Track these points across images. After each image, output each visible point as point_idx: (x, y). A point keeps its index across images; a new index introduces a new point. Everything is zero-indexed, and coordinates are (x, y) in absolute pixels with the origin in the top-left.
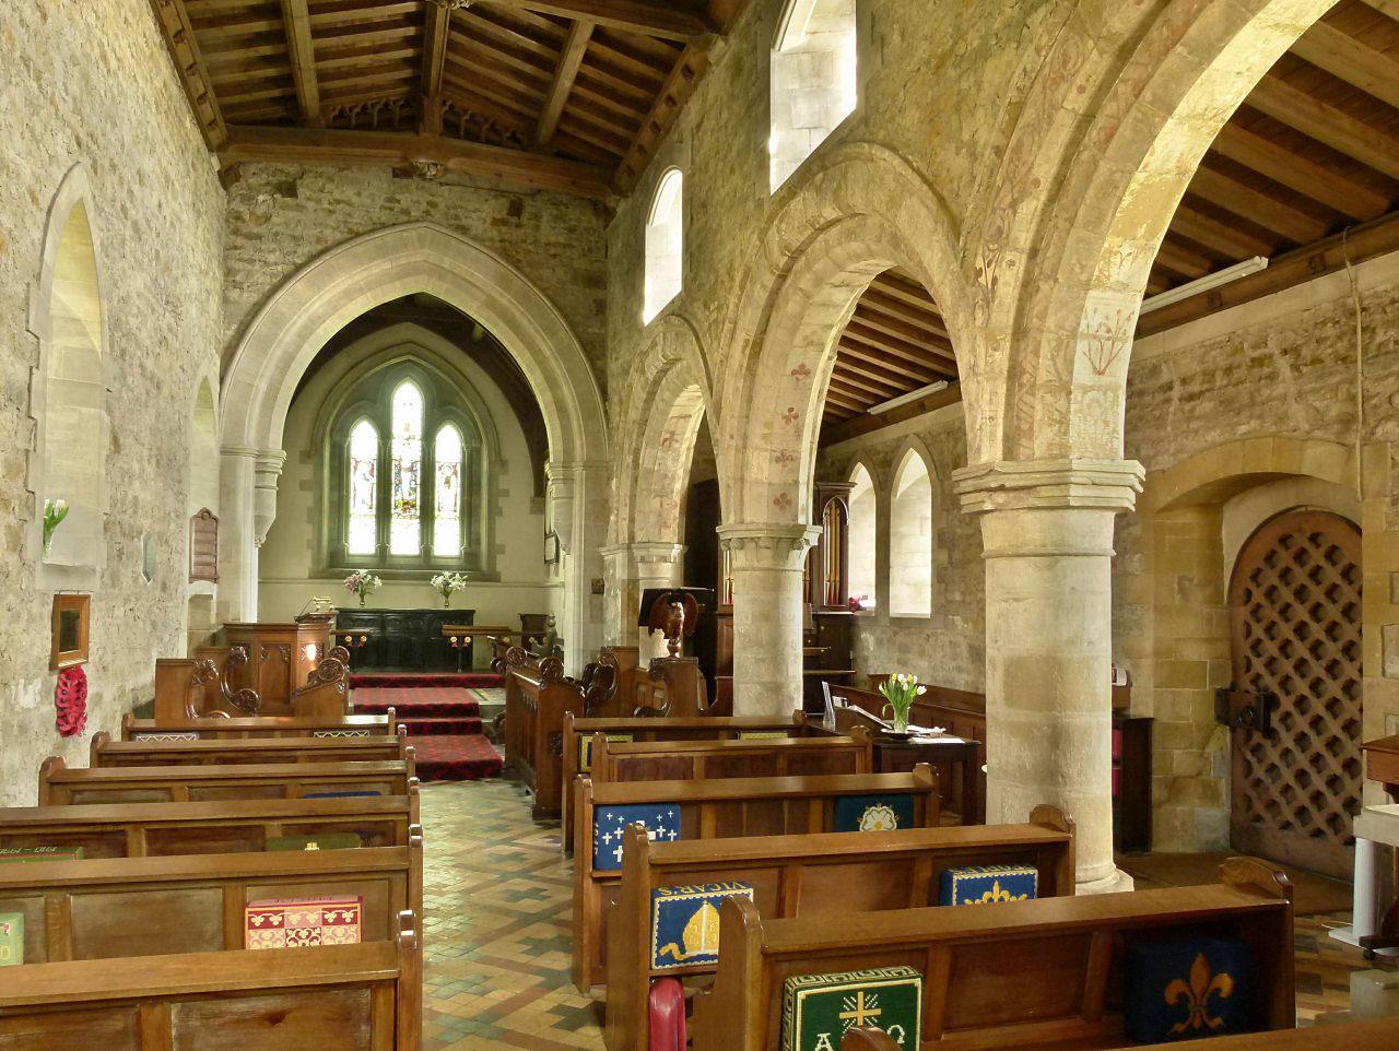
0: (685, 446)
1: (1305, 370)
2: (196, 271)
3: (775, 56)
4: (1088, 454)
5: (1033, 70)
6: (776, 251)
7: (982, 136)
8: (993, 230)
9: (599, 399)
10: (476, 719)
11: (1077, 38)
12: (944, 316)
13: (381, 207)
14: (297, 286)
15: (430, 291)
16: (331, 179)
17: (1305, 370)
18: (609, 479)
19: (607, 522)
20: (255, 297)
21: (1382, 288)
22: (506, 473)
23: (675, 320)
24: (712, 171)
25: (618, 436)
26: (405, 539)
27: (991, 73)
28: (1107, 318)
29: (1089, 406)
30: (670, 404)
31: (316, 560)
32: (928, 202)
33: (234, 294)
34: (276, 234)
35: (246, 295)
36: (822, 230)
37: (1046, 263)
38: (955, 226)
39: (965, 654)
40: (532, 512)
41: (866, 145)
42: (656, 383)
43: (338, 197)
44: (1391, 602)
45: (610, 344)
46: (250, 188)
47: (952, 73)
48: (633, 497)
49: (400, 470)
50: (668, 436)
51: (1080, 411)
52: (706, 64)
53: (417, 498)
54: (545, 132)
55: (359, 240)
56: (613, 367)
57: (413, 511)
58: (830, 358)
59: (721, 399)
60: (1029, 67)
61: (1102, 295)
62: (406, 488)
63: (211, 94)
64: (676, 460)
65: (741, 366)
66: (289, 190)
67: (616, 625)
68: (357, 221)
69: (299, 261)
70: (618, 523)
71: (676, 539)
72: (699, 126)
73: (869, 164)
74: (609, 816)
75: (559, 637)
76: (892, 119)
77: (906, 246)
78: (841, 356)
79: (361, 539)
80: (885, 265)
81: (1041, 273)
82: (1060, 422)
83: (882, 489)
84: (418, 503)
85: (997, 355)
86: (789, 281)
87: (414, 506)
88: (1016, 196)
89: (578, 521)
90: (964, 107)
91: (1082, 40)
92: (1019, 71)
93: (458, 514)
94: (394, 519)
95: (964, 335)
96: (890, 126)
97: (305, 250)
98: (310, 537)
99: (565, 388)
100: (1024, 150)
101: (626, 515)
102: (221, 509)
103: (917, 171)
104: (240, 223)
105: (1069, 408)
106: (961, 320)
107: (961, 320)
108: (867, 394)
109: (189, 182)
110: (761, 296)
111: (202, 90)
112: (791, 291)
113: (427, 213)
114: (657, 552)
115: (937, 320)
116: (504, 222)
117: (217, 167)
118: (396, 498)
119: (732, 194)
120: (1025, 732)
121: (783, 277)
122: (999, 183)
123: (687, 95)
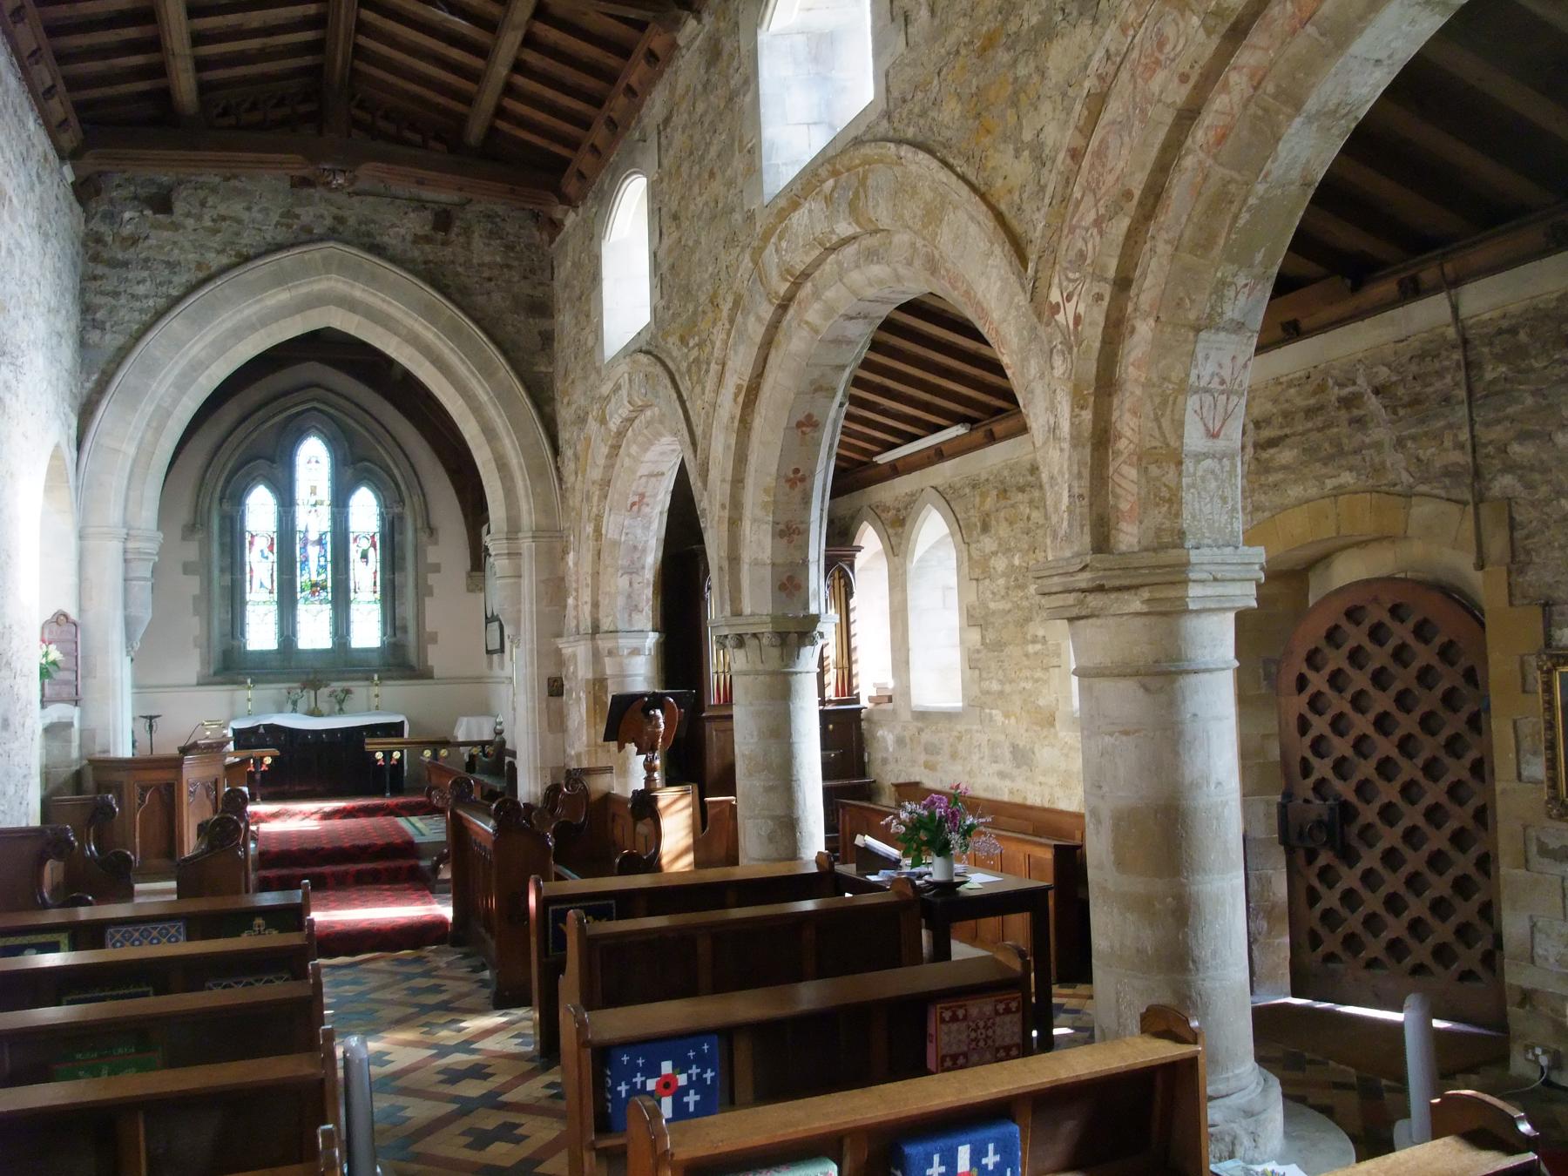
0: (658, 509)
1: (1401, 412)
2: (43, 309)
3: (763, 37)
4: (1206, 541)
5: (1117, 54)
6: (774, 274)
7: (1051, 135)
8: (1072, 254)
9: (548, 453)
10: (412, 862)
11: (1175, 13)
12: (1005, 360)
13: (278, 224)
14: (173, 324)
15: (337, 324)
16: (214, 190)
17: (1401, 412)
18: (565, 552)
19: (565, 607)
20: (120, 340)
21: (1486, 316)
22: (436, 543)
23: (644, 359)
24: (685, 176)
25: (575, 500)
26: (314, 632)
27: (1059, 57)
28: (1220, 366)
29: (1203, 479)
30: (637, 460)
31: (205, 662)
32: (981, 218)
33: (94, 336)
34: (146, 260)
35: (108, 337)
36: (833, 249)
37: (1143, 298)
38: (1018, 247)
39: (1008, 756)
40: (469, 590)
41: (892, 145)
42: (621, 434)
43: (223, 212)
44: (1524, 691)
45: (559, 385)
46: (111, 201)
47: (1004, 57)
48: (596, 574)
49: (305, 546)
50: (636, 499)
51: (1193, 485)
52: (674, 46)
53: (328, 576)
54: (475, 131)
55: (250, 265)
56: (565, 414)
57: (323, 594)
58: (841, 405)
59: (707, 458)
60: (1112, 50)
61: (1213, 337)
62: (314, 565)
63: (61, 87)
64: (646, 528)
65: (733, 418)
66: (162, 203)
67: (583, 735)
68: (248, 240)
69: (175, 293)
70: (578, 607)
71: (649, 626)
72: (667, 121)
73: (896, 168)
74: (625, 1058)
75: (508, 746)
76: (923, 113)
77: (947, 271)
78: (854, 401)
79: (261, 634)
80: (914, 288)
81: (1135, 310)
82: (1170, 501)
83: (895, 555)
84: (329, 584)
85: (1084, 413)
86: (791, 311)
87: (324, 588)
88: (1102, 211)
89: (528, 607)
90: (1022, 96)
91: (1183, 15)
92: (1100, 54)
93: (378, 596)
94: (301, 607)
95: (1038, 388)
96: (922, 122)
97: (182, 279)
98: (197, 633)
99: (507, 441)
100: (1111, 153)
101: (588, 599)
102: (81, 610)
103: (962, 178)
104: (100, 248)
105: (1180, 482)
106: (1033, 368)
107: (1033, 368)
108: (873, 440)
109: (33, 198)
110: (756, 331)
111: (49, 83)
112: (794, 324)
113: (333, 230)
114: (625, 643)
115: (997, 368)
116: (427, 239)
117: (70, 177)
118: (302, 579)
119: (712, 205)
120: (1144, 907)
121: (783, 307)
122: (1077, 194)
123: (650, 83)
